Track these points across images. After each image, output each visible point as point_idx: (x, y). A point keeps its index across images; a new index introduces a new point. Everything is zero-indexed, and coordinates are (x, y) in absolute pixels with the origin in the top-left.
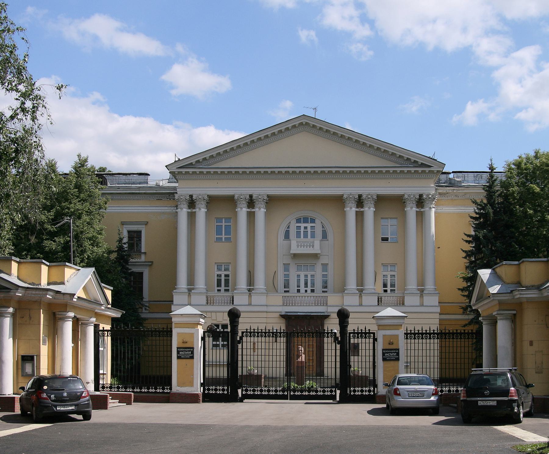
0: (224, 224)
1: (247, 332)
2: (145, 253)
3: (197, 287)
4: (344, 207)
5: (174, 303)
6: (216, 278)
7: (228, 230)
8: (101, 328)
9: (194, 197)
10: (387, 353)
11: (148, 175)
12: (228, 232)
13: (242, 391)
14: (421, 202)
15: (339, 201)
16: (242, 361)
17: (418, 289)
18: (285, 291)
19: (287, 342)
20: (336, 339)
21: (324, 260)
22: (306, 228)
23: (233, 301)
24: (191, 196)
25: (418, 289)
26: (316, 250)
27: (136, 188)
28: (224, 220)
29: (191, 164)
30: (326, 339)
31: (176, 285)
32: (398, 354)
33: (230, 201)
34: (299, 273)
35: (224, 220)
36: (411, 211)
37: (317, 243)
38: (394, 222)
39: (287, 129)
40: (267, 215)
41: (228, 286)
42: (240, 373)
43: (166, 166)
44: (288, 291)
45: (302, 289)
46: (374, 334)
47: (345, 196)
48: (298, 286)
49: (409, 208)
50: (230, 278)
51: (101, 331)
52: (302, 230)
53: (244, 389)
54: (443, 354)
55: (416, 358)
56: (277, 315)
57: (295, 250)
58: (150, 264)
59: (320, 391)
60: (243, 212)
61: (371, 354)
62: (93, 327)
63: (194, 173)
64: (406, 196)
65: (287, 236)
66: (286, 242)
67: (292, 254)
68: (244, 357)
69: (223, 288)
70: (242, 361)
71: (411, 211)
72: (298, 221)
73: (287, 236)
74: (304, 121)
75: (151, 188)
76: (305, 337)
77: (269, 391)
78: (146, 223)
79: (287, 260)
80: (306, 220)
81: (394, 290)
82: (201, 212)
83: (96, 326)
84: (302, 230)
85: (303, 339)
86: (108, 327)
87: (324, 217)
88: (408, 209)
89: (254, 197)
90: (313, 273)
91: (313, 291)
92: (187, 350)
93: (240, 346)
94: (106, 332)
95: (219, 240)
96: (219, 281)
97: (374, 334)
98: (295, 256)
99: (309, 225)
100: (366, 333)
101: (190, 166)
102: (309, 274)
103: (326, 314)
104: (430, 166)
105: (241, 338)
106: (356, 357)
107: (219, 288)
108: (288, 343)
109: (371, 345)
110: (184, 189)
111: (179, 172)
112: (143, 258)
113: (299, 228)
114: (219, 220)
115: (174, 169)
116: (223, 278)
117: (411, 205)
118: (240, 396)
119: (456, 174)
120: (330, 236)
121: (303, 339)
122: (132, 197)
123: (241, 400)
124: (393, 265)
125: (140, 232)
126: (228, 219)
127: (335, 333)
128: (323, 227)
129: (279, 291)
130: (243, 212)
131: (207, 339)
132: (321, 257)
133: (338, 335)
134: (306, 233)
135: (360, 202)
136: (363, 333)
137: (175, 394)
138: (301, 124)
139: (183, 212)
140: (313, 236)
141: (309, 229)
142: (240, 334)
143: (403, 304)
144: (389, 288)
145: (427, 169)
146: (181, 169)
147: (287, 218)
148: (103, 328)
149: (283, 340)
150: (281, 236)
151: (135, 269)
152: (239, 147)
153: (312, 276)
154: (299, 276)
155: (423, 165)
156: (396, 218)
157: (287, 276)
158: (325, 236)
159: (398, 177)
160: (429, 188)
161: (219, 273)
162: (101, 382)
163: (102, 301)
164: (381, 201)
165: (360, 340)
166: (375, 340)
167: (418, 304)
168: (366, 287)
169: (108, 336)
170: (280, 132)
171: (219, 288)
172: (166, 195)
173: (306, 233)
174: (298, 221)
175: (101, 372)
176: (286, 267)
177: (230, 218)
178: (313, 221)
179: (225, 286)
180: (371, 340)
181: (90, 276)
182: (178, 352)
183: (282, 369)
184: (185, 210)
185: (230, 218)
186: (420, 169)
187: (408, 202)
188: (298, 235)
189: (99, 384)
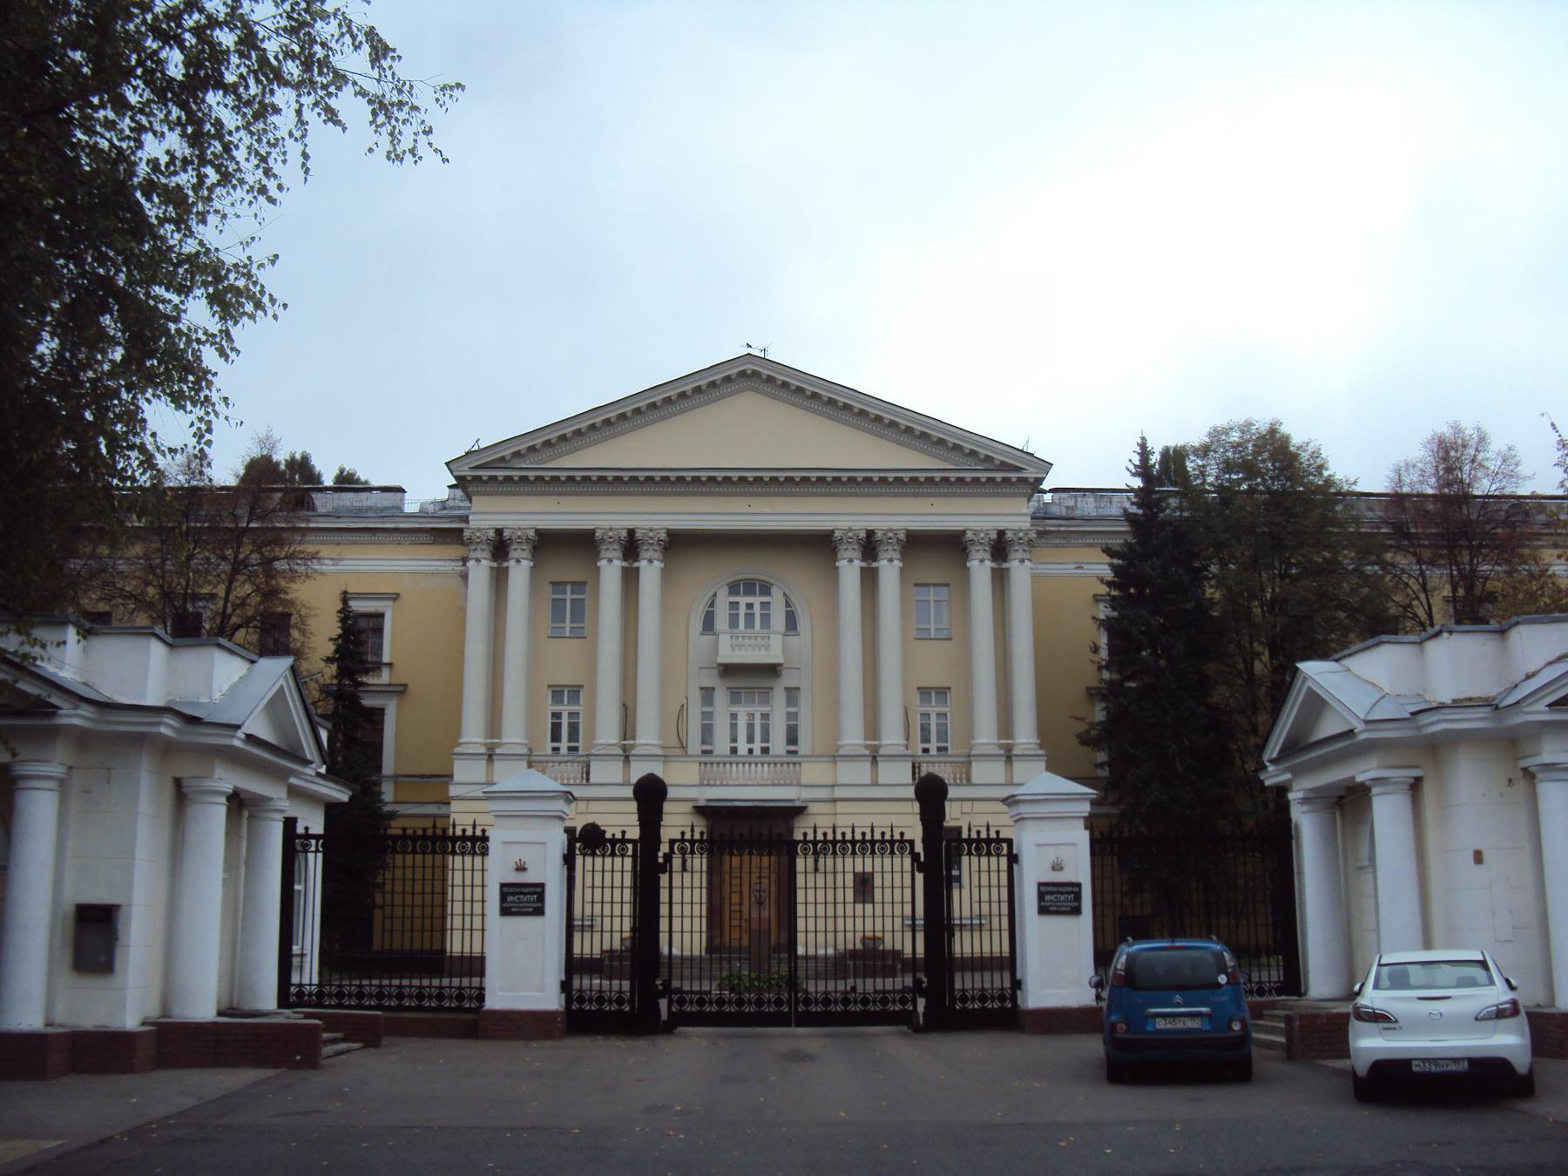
0: (569, 597)
1: (683, 840)
2: (390, 665)
3: (505, 740)
4: (836, 560)
5: (456, 778)
6: (550, 720)
7: (578, 607)
8: (300, 830)
9: (506, 534)
11: (400, 490)
12: (578, 615)
15: (821, 545)
17: (1001, 746)
19: (710, 872)
20: (915, 857)
21: (788, 679)
22: (750, 606)
23: (588, 774)
24: (499, 532)
25: (1001, 746)
26: (773, 655)
27: (375, 517)
28: (569, 588)
29: (503, 459)
30: (800, 862)
31: (459, 736)
33: (584, 543)
34: (734, 709)
35: (569, 588)
36: (980, 569)
37: (776, 641)
38: (943, 593)
43: (447, 464)
45: (743, 747)
46: (1010, 842)
47: (837, 534)
48: (734, 740)
49: (976, 563)
51: (300, 836)
52: (742, 610)
53: (675, 997)
54: (438, 889)
55: (468, 890)
56: (688, 807)
57: (728, 655)
58: (400, 691)
60: (611, 570)
61: (1004, 896)
62: (281, 825)
63: (508, 479)
64: (969, 535)
65: (709, 624)
66: (708, 638)
67: (720, 665)
68: (676, 910)
69: (564, 745)
71: (980, 569)
72: (734, 589)
73: (709, 624)
74: (749, 367)
78: (395, 597)
79: (711, 680)
80: (750, 587)
81: (946, 749)
83: (290, 823)
84: (742, 610)
85: (887, 860)
86: (318, 827)
87: (792, 580)
88: (973, 564)
90: (765, 709)
91: (765, 751)
93: (664, 878)
94: (313, 842)
96: (556, 728)
97: (1010, 842)
98: (728, 670)
99: (756, 600)
100: (988, 841)
102: (758, 710)
103: (797, 804)
104: (1020, 469)
106: (869, 907)
107: (556, 745)
110: (487, 514)
112: (385, 677)
113: (734, 605)
114: (558, 585)
115: (465, 471)
116: (565, 721)
117: (981, 555)
118: (664, 1016)
119: (1057, 496)
120: (803, 624)
121: (887, 860)
122: (366, 537)
123: (668, 1028)
125: (382, 616)
126: (579, 586)
127: (912, 842)
128: (787, 604)
130: (611, 570)
133: (919, 848)
134: (750, 617)
135: (870, 546)
138: (742, 374)
139: (480, 571)
141: (757, 610)
142: (664, 848)
145: (1014, 476)
146: (480, 474)
147: (708, 580)
148: (307, 829)
149: (699, 862)
151: (367, 702)
152: (607, 422)
153: (765, 716)
154: (734, 716)
155: (1004, 467)
156: (947, 585)
157: (707, 715)
158: (791, 623)
159: (942, 499)
160: (1013, 515)
161: (557, 708)
162: (295, 979)
163: (310, 751)
164: (917, 544)
166: (1013, 859)
167: (1002, 780)
169: (317, 851)
170: (698, 390)
171: (556, 745)
172: (443, 532)
173: (750, 617)
174: (734, 589)
175: (296, 949)
176: (708, 693)
178: (766, 589)
180: (1004, 861)
181: (282, 682)
183: (696, 936)
184: (484, 562)
186: (999, 476)
187: (973, 549)
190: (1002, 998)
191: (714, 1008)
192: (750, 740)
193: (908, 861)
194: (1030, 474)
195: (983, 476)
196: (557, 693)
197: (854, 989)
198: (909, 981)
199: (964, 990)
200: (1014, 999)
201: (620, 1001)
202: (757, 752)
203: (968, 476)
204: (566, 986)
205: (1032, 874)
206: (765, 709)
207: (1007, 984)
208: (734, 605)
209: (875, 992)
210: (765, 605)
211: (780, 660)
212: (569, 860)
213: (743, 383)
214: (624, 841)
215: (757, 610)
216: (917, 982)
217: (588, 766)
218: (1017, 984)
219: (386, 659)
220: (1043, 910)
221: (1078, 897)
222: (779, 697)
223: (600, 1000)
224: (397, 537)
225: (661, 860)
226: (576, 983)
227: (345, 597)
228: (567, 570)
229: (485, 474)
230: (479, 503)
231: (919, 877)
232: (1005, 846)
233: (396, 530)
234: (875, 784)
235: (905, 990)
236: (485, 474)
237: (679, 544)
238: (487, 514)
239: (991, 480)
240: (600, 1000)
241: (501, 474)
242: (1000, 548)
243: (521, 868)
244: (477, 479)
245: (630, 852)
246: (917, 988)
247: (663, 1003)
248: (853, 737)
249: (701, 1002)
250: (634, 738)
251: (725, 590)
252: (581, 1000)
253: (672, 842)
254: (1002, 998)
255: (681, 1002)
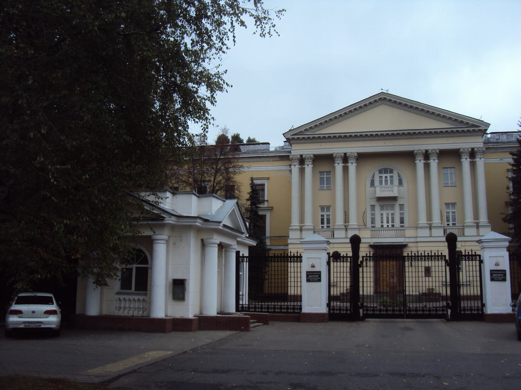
0: (325, 176)
1: (367, 256)
2: (267, 201)
5: (290, 237)
6: (320, 217)
9: (304, 156)
10: (311, 275)
11: (268, 144)
12: (328, 182)
13: (363, 311)
14: (473, 154)
16: (363, 282)
17: (475, 223)
18: (372, 227)
20: (446, 261)
21: (400, 201)
22: (386, 177)
23: (333, 235)
25: (475, 223)
29: (301, 132)
31: (291, 223)
32: (320, 276)
33: (330, 158)
34: (382, 212)
36: (466, 162)
37: (396, 189)
39: (370, 103)
40: (357, 167)
41: (329, 224)
42: (361, 293)
44: (374, 227)
45: (385, 225)
46: (480, 256)
48: (382, 222)
50: (331, 217)
51: (241, 257)
52: (384, 179)
53: (365, 309)
56: (367, 245)
57: (379, 194)
58: (271, 209)
59: (433, 310)
60: (339, 167)
62: (235, 254)
64: (461, 150)
65: (372, 184)
66: (373, 189)
68: (365, 280)
69: (325, 225)
70: (363, 282)
71: (466, 162)
72: (380, 172)
73: (372, 184)
74: (382, 97)
75: (272, 152)
76: (438, 260)
77: (393, 310)
78: (268, 179)
79: (374, 202)
80: (386, 171)
82: (309, 168)
83: (238, 253)
84: (384, 179)
87: (400, 168)
88: (463, 160)
89: (348, 155)
90: (392, 212)
91: (393, 226)
92: (500, 272)
93: (361, 269)
95: (322, 189)
96: (322, 220)
97: (480, 256)
98: (380, 199)
99: (388, 175)
100: (472, 255)
101: (301, 133)
102: (390, 212)
103: (404, 244)
104: (479, 126)
105: (362, 262)
108: (376, 267)
109: (478, 268)
110: (297, 150)
111: (293, 138)
112: (266, 205)
113: (381, 177)
114: (321, 173)
115: (289, 136)
116: (325, 218)
117: (466, 157)
118: (361, 315)
119: (492, 135)
120: (405, 183)
122: (258, 159)
123: (363, 319)
124: (454, 204)
125: (264, 185)
126: (328, 172)
127: (445, 256)
128: (399, 176)
129: (368, 227)
130: (339, 167)
131: (332, 264)
132: (399, 199)
134: (386, 181)
136: (470, 255)
137: (305, 314)
138: (380, 99)
139: (295, 169)
140: (392, 181)
142: (361, 259)
143: (464, 234)
144: (451, 223)
145: (476, 129)
146: (294, 137)
147: (371, 169)
150: (368, 184)
151: (261, 213)
153: (392, 214)
154: (382, 214)
155: (473, 126)
156: (454, 168)
157: (373, 214)
158: (400, 183)
160: (477, 143)
161: (323, 213)
162: (241, 303)
164: (443, 154)
165: (430, 262)
166: (481, 262)
168: (434, 222)
169: (247, 261)
172: (283, 157)
173: (386, 181)
174: (380, 172)
175: (241, 293)
176: (373, 207)
177: (330, 172)
178: (391, 171)
179: (327, 224)
180: (478, 262)
182: (307, 276)
184: (297, 166)
185: (330, 172)
186: (471, 129)
187: (463, 155)
188: (381, 182)
189: (239, 304)
190: (478, 310)
191: (378, 312)
192: (388, 222)
193: (444, 262)
194: (483, 128)
195: (466, 129)
196: (322, 208)
197: (426, 306)
198: (445, 303)
199: (464, 307)
200: (482, 310)
201: (347, 310)
202: (390, 226)
203: (460, 130)
204: (328, 305)
205: (488, 266)
206: (392, 212)
207: (480, 305)
208: (381, 177)
209: (433, 307)
210: (391, 177)
211: (397, 195)
212: (329, 263)
213: (381, 102)
214: (347, 257)
215: (389, 179)
216: (448, 304)
217: (334, 232)
218: (483, 305)
219: (266, 199)
220: (492, 279)
221: (505, 275)
222: (397, 208)
223: (340, 310)
224: (268, 159)
225: (359, 263)
226: (332, 304)
227: (252, 179)
228: (324, 167)
229: (296, 137)
230: (294, 147)
231: (448, 268)
232: (478, 257)
233: (267, 157)
234: (431, 236)
235: (443, 307)
236: (296, 137)
237: (362, 157)
238: (297, 150)
239: (468, 131)
240: (340, 310)
241: (301, 137)
242: (473, 154)
243: (313, 266)
244: (293, 139)
245: (349, 261)
246: (448, 306)
247: (361, 311)
248: (423, 220)
249: (374, 310)
250: (348, 222)
251: (378, 172)
252: (334, 309)
253: (363, 257)
254: (478, 310)
255: (367, 310)
